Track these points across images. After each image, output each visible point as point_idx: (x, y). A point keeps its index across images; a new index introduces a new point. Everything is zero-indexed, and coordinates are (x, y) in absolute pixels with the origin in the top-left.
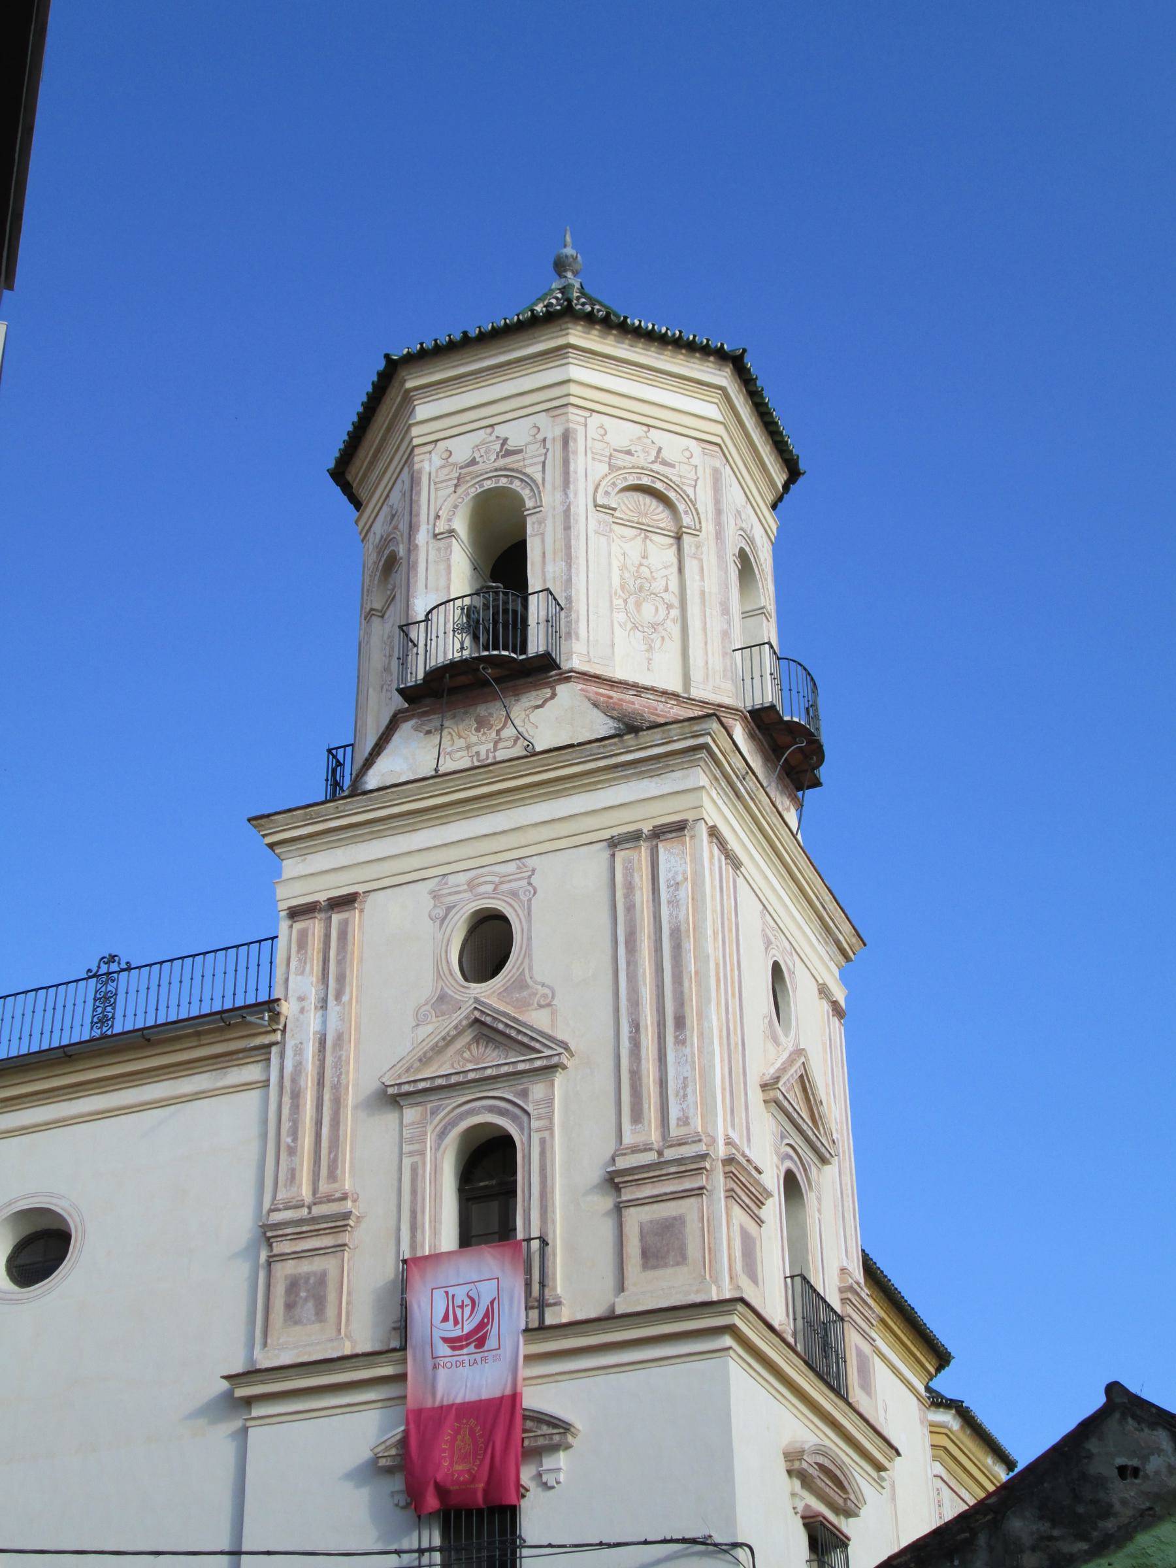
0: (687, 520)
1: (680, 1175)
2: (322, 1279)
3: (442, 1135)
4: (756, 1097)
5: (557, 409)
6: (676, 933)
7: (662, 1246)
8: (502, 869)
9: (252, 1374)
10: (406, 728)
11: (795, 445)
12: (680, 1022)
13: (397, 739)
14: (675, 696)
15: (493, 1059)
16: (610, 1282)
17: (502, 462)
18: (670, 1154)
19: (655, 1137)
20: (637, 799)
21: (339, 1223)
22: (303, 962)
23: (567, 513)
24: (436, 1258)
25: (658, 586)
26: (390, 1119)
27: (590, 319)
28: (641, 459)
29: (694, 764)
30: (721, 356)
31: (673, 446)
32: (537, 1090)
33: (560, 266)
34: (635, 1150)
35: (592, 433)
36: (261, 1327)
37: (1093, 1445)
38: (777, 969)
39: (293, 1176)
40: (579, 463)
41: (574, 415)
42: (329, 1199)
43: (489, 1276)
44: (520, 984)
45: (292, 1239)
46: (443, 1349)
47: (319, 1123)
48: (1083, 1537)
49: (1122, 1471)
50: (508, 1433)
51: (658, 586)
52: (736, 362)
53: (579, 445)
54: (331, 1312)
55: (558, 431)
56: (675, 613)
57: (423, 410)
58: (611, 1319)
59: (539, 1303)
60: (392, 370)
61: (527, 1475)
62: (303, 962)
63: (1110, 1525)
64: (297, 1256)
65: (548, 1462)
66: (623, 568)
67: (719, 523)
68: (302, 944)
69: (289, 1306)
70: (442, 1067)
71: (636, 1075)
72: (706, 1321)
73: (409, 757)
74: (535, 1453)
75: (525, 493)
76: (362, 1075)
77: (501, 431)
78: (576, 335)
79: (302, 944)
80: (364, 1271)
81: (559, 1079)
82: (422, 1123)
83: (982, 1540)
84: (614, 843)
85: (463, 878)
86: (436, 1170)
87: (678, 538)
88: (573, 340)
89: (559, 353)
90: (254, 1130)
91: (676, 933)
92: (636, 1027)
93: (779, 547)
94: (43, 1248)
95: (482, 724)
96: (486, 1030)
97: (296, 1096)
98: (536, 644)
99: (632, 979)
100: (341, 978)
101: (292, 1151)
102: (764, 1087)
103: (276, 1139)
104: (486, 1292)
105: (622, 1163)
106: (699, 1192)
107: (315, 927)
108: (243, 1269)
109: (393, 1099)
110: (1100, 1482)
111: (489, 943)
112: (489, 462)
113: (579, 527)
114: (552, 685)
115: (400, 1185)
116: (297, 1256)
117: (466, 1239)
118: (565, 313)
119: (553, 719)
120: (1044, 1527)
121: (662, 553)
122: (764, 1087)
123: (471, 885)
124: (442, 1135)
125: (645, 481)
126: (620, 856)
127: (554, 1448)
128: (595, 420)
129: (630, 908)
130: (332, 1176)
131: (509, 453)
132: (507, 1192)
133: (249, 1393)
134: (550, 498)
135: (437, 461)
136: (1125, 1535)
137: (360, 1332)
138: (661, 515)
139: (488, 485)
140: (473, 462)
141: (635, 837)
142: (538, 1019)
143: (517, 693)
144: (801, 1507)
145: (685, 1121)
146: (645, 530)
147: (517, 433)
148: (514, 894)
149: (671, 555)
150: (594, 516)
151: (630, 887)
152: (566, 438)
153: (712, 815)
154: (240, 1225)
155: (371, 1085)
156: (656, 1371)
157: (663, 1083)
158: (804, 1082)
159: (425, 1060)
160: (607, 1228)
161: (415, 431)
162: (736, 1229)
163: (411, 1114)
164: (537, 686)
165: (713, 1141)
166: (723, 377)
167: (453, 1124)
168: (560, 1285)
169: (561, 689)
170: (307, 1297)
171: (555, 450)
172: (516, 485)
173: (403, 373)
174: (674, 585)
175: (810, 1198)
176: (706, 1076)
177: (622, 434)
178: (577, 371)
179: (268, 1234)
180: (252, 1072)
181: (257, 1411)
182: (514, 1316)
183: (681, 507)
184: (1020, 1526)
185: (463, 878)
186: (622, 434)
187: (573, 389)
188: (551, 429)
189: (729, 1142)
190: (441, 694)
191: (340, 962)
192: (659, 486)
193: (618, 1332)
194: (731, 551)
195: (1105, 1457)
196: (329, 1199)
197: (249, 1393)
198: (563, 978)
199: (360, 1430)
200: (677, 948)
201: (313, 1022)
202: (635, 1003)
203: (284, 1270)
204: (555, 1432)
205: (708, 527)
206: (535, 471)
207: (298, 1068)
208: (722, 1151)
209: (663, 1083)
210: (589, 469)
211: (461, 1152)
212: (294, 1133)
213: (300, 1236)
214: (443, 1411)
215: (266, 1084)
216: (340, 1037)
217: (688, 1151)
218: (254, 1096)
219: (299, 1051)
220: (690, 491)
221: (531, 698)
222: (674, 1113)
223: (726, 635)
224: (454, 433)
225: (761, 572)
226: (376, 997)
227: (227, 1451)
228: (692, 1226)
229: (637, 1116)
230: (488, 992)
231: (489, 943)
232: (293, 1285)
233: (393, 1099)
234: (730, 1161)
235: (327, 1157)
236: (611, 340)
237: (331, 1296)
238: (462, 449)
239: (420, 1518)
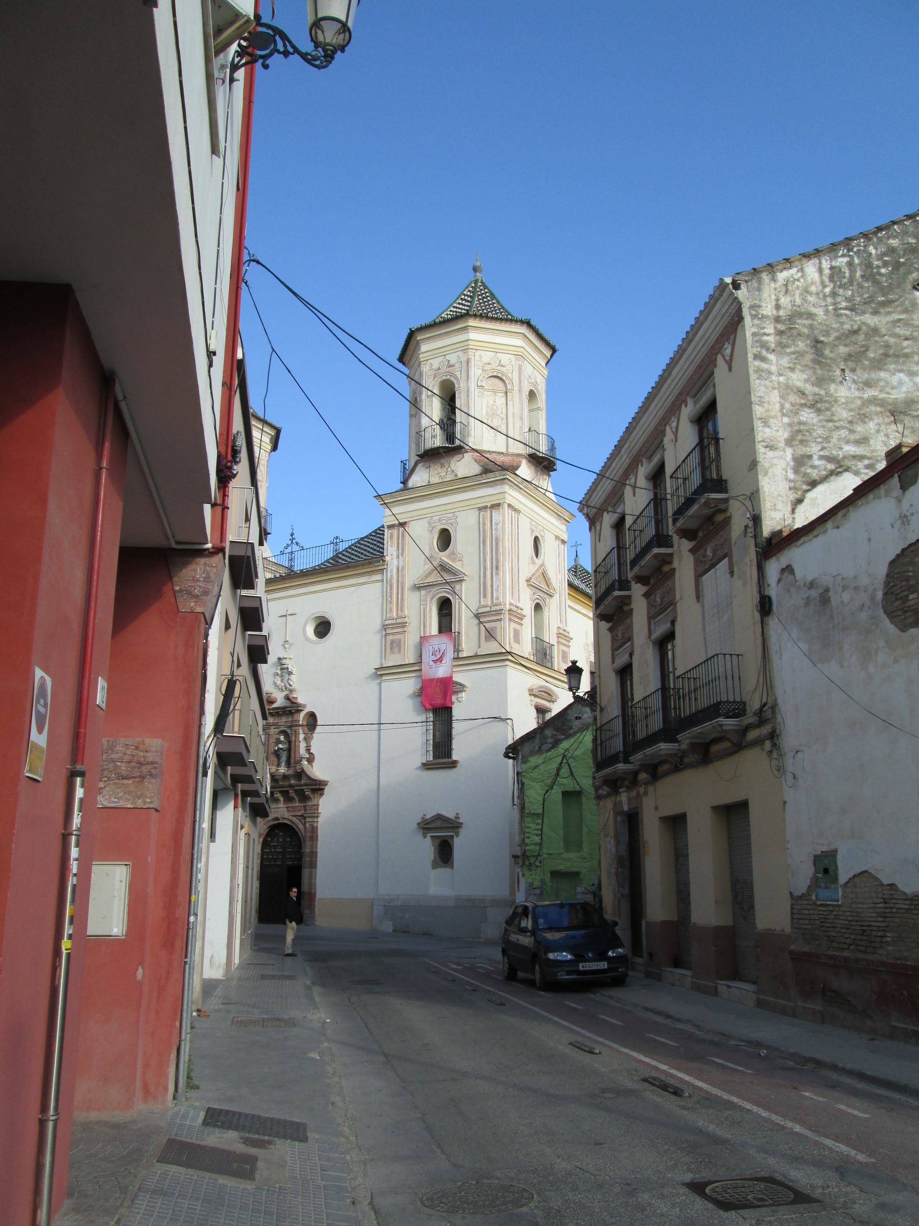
0: (509, 387)
1: (496, 615)
2: (400, 641)
3: (432, 599)
4: (523, 585)
5: (465, 351)
6: (497, 539)
7: (491, 635)
8: (449, 515)
9: (382, 668)
10: (420, 466)
11: (552, 342)
12: (497, 568)
13: (417, 469)
14: (502, 453)
15: (448, 577)
16: (477, 645)
17: (448, 369)
18: (493, 608)
19: (489, 603)
20: (486, 494)
21: (403, 625)
22: (392, 543)
23: (468, 390)
24: (431, 636)
25: (499, 412)
26: (417, 594)
27: (475, 316)
28: (494, 366)
29: (504, 483)
30: (522, 322)
31: (505, 358)
32: (457, 587)
33: (475, 269)
34: (484, 606)
35: (477, 358)
36: (383, 654)
37: (569, 712)
38: (536, 540)
39: (391, 610)
40: (472, 371)
41: (471, 352)
42: (401, 617)
43: (444, 644)
44: (453, 553)
45: (392, 629)
46: (432, 663)
47: (398, 594)
48: (564, 734)
49: (577, 718)
50: (447, 686)
51: (499, 412)
52: (528, 324)
53: (472, 364)
54: (402, 650)
55: (465, 359)
56: (504, 421)
57: (424, 348)
58: (476, 656)
59: (457, 650)
60: (411, 334)
61: (454, 698)
62: (392, 543)
63: (571, 731)
64: (393, 634)
65: (460, 695)
66: (487, 407)
67: (520, 386)
68: (391, 537)
69: (391, 648)
70: (431, 579)
71: (485, 583)
72: (503, 657)
73: (419, 478)
74: (457, 692)
75: (455, 382)
76: (409, 582)
77: (448, 357)
78: (471, 322)
79: (391, 537)
80: (411, 639)
81: (464, 583)
82: (426, 595)
83: (538, 736)
84: (480, 509)
85: (437, 518)
86: (430, 609)
87: (506, 393)
88: (470, 324)
89: (465, 328)
90: (380, 595)
91: (497, 539)
92: (485, 568)
93: (549, 381)
94: (323, 628)
95: (442, 466)
96: (444, 568)
97: (391, 585)
98: (457, 443)
99: (484, 554)
100: (403, 549)
101: (391, 602)
102: (527, 581)
103: (386, 598)
104: (443, 647)
105: (481, 611)
106: (500, 620)
107: (395, 531)
108: (378, 636)
109: (418, 588)
110: (570, 721)
111: (445, 539)
112: (444, 369)
113: (472, 395)
114: (463, 454)
115: (422, 616)
116: (393, 634)
117: (440, 631)
118: (467, 315)
119: (465, 466)
120: (554, 732)
121: (500, 399)
122: (527, 581)
123: (440, 520)
124: (432, 599)
125: (495, 374)
126: (482, 513)
127: (461, 691)
128: (478, 353)
129: (484, 531)
130: (402, 611)
131: (450, 366)
132: (450, 615)
133: (381, 673)
134: (463, 384)
135: (428, 368)
136: (575, 734)
137: (410, 658)
138: (501, 384)
139: (444, 378)
140: (439, 369)
141: (486, 507)
142: (457, 566)
143: (453, 456)
144: (534, 703)
145: (497, 598)
146: (495, 392)
147: (453, 358)
148: (451, 524)
149: (504, 400)
150: (477, 390)
151: (484, 524)
152: (468, 361)
153: (509, 500)
154: (378, 624)
155: (412, 583)
156: (489, 671)
157: (492, 586)
158: (544, 575)
159: (426, 577)
160: (476, 629)
161: (421, 356)
162: (512, 630)
163: (423, 592)
164: (459, 454)
165: (505, 605)
166: (523, 329)
167: (435, 596)
168: (464, 645)
169: (465, 455)
170: (396, 646)
171: (464, 365)
172: (452, 379)
173: (416, 334)
174: (504, 412)
175: (546, 610)
176: (504, 585)
177: (487, 357)
178: (472, 335)
179: (385, 627)
180: (378, 577)
181: (384, 678)
182: (450, 654)
183: (507, 382)
184: (548, 732)
185: (437, 518)
186: (487, 357)
187: (470, 343)
188: (464, 359)
189: (511, 604)
190: (431, 456)
191: (403, 544)
192: (500, 375)
193: (478, 659)
194: (526, 393)
195: (572, 715)
196: (401, 617)
197: (381, 673)
198: (466, 554)
199: (408, 685)
200: (497, 544)
201: (395, 564)
202: (485, 561)
203: (390, 638)
204: (462, 687)
205: (516, 388)
206: (458, 374)
207: (391, 576)
208: (508, 607)
209: (492, 586)
210: (476, 372)
211: (438, 603)
212: (391, 597)
213: (393, 628)
214: (431, 680)
215: (383, 581)
216: (403, 568)
217: (498, 608)
218: (379, 584)
219: (391, 572)
220: (510, 375)
221: (457, 457)
222: (495, 596)
223: (521, 428)
224: (434, 353)
225: (539, 394)
226: (409, 558)
227: (376, 688)
228: (499, 627)
229: (485, 596)
230: (444, 556)
231: (445, 539)
232: (392, 642)
233: (418, 588)
234: (510, 610)
235: (400, 606)
236: (483, 322)
237: (402, 646)
238: (436, 363)
239: (426, 710)
